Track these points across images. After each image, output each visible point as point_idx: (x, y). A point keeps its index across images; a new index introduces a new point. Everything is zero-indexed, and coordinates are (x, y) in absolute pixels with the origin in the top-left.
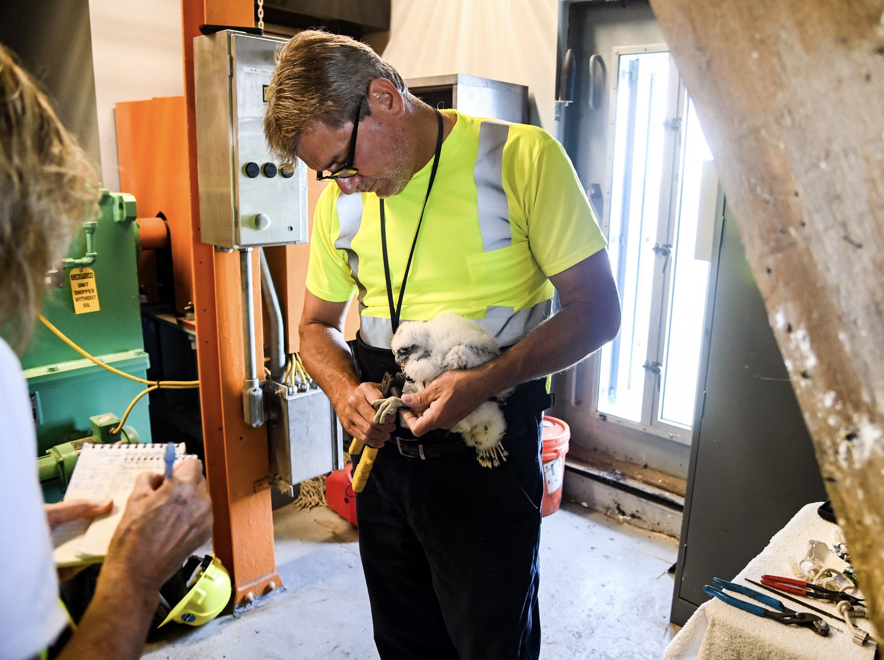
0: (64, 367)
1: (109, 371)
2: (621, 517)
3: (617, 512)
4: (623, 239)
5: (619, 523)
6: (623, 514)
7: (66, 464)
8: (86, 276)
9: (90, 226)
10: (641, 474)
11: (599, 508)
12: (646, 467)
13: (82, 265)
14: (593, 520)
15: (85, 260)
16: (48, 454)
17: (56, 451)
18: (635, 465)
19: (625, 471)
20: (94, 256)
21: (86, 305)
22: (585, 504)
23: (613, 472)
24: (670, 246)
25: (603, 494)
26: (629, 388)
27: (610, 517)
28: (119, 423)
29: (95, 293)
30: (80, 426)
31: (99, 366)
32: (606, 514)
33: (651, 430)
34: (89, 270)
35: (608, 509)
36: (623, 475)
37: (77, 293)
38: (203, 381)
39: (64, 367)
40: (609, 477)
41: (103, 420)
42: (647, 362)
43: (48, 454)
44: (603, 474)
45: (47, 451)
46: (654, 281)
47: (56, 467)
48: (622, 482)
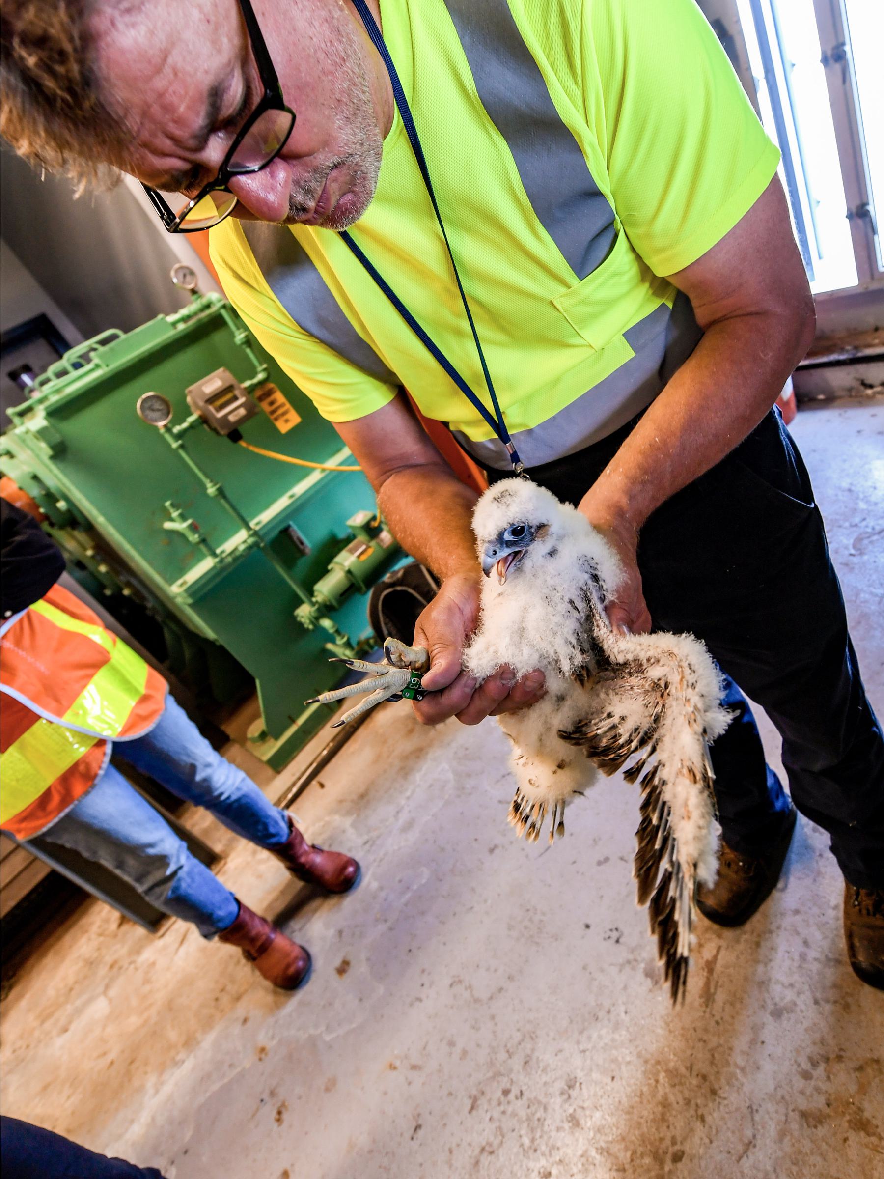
0: (300, 488)
1: (342, 472)
2: (869, 392)
3: (862, 388)
4: (770, 76)
5: (870, 398)
6: (871, 386)
7: (353, 569)
8: (269, 393)
9: (244, 340)
10: (875, 338)
11: (839, 393)
12: (877, 329)
13: (261, 383)
14: (839, 407)
15: (261, 376)
16: (332, 569)
17: (337, 563)
18: (863, 333)
19: (857, 343)
20: (265, 370)
21: (287, 421)
22: (821, 397)
23: (842, 350)
24: (843, 44)
25: (839, 378)
26: (820, 258)
27: (856, 397)
28: (775, 180)
29: (288, 406)
30: (341, 535)
31: (332, 471)
32: (851, 396)
33: (874, 286)
34: (271, 385)
35: (850, 390)
36: (856, 348)
37: (273, 412)
38: (126, 340)
39: (300, 488)
40: (842, 357)
41: (359, 519)
42: (848, 210)
43: (332, 569)
44: (833, 357)
45: (329, 567)
46: (832, 105)
47: (346, 576)
48: (860, 354)
